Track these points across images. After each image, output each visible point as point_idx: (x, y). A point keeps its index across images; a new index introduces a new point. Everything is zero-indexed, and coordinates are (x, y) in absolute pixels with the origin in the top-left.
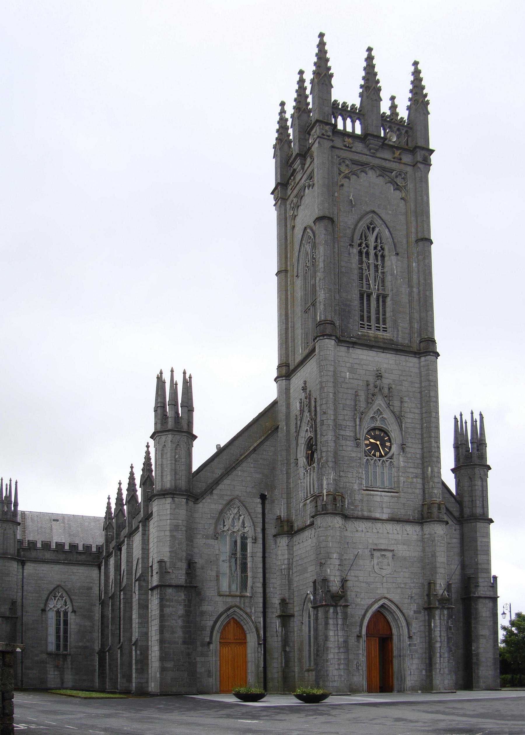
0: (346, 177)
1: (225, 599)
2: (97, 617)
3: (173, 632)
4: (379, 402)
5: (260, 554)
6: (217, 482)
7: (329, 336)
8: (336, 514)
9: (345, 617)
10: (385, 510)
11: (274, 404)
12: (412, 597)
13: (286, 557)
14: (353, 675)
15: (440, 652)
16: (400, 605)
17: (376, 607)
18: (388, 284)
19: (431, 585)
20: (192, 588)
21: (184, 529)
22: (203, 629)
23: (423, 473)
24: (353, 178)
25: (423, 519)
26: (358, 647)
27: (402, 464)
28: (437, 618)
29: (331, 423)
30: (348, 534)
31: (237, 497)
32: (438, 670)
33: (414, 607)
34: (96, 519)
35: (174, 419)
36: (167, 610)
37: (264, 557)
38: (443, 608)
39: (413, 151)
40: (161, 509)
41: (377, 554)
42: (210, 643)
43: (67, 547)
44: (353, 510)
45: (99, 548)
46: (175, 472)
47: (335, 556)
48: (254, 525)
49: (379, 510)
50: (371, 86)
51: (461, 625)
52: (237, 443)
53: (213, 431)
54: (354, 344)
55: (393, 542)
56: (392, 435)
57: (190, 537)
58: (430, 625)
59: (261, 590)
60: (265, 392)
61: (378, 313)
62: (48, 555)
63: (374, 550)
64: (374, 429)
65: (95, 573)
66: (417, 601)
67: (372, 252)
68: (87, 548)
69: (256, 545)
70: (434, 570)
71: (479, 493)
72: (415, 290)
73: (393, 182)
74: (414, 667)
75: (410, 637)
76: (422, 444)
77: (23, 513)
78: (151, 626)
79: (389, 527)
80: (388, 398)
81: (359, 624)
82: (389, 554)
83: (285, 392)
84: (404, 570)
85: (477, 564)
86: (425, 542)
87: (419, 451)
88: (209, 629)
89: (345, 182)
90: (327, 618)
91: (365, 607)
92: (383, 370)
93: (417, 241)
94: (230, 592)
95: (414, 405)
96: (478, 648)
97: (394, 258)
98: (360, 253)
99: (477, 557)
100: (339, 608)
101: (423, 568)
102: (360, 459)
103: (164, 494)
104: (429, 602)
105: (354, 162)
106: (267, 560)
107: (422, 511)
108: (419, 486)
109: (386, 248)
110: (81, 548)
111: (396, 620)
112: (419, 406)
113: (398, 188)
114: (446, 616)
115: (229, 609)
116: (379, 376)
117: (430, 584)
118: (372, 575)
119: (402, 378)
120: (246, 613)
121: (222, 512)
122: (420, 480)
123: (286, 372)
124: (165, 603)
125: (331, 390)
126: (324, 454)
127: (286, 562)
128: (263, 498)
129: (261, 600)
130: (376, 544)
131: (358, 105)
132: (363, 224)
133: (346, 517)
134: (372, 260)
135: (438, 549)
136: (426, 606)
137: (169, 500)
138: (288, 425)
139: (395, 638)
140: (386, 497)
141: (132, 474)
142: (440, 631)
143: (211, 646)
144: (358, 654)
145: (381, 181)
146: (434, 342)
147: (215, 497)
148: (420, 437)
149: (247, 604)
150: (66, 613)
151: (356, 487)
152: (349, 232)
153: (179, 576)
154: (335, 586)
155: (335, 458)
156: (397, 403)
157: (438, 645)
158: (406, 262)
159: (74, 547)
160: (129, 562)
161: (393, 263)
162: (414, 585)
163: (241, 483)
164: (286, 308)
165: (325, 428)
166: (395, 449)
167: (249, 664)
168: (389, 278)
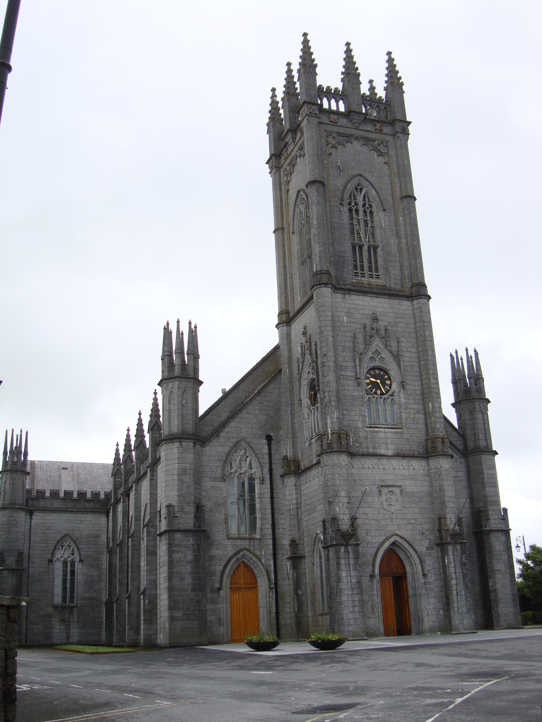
0: (334, 147)
2: (105, 566)
3: (182, 579)
4: (377, 343)
5: (268, 495)
6: (224, 425)
7: (326, 284)
10: (390, 446)
11: (277, 348)
12: (423, 533)
14: (368, 618)
16: (412, 542)
19: (441, 519)
20: (201, 532)
21: (192, 472)
22: (212, 574)
24: (341, 159)
25: (428, 453)
27: (403, 401)
28: (450, 553)
29: (332, 364)
30: (355, 471)
32: (456, 609)
33: (426, 543)
34: (104, 466)
35: (180, 366)
36: (176, 556)
37: (272, 498)
38: (456, 543)
39: (392, 123)
40: (169, 454)
41: (385, 490)
42: (220, 589)
43: (75, 495)
44: (358, 447)
45: (107, 495)
46: (182, 417)
47: (343, 494)
48: (261, 466)
49: (384, 446)
50: (351, 72)
51: (476, 560)
52: (241, 386)
53: (218, 377)
54: (349, 291)
55: (400, 478)
56: (392, 373)
57: (198, 481)
58: (444, 562)
59: (270, 531)
60: (269, 338)
61: (370, 262)
62: (56, 504)
63: (382, 486)
64: (374, 368)
65: (103, 520)
66: (429, 537)
67: (361, 209)
68: (96, 495)
70: (443, 504)
71: (480, 426)
74: (431, 607)
75: (424, 575)
76: (421, 380)
77: (33, 463)
78: (160, 573)
79: (395, 462)
81: (371, 563)
82: (397, 490)
83: (286, 337)
85: (485, 496)
86: (432, 477)
87: (419, 388)
88: (218, 574)
89: (333, 151)
90: (338, 558)
91: (377, 545)
92: (378, 314)
93: (402, 198)
94: (239, 535)
95: (410, 345)
96: (495, 583)
97: (381, 214)
98: (350, 210)
99: (485, 490)
100: (350, 547)
101: (432, 503)
102: (362, 397)
103: (171, 438)
104: (441, 538)
106: (276, 501)
107: (427, 446)
108: (422, 421)
109: (374, 205)
110: (89, 496)
111: (409, 557)
112: (415, 345)
113: (380, 154)
114: (459, 551)
115: (238, 552)
116: (375, 319)
117: (440, 518)
118: (381, 512)
119: (397, 320)
120: (256, 556)
121: (228, 454)
122: (422, 416)
123: (286, 319)
124: (173, 548)
125: (330, 333)
126: (327, 394)
128: (269, 438)
129: (270, 542)
130: (383, 481)
131: (340, 88)
132: (351, 186)
133: (351, 455)
134: (361, 216)
135: (445, 483)
136: (438, 542)
137: (177, 444)
138: (290, 368)
139: (409, 576)
140: (390, 434)
141: (140, 420)
143: (221, 592)
144: (372, 595)
145: (365, 149)
146: (425, 286)
147: (222, 440)
148: (418, 374)
149: (257, 547)
150: (73, 563)
151: (360, 425)
152: (339, 193)
153: (187, 521)
156: (394, 344)
157: (454, 582)
159: (82, 494)
160: (137, 508)
161: (381, 219)
163: (247, 425)
164: (284, 261)
165: (326, 369)
168: (378, 231)
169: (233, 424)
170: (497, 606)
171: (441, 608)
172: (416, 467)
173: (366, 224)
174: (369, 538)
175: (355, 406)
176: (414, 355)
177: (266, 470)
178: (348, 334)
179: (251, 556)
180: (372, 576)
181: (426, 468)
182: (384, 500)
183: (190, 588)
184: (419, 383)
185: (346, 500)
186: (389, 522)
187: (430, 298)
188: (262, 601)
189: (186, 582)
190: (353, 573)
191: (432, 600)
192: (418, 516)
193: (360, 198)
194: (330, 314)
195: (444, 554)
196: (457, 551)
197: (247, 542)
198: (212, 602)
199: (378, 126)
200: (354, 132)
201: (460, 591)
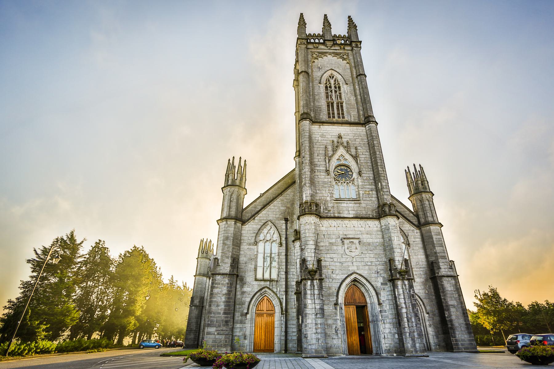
1: (259, 283)
3: (218, 306)
4: (341, 151)
5: (284, 254)
6: (258, 213)
8: (312, 214)
9: (321, 288)
10: (350, 212)
11: (294, 170)
12: (378, 272)
13: (299, 254)
14: (332, 339)
15: (407, 317)
16: (369, 279)
17: (348, 280)
18: (343, 97)
19: (391, 261)
21: (232, 238)
22: (243, 303)
23: (376, 188)
25: (379, 215)
26: (336, 314)
27: (360, 184)
28: (400, 287)
29: (308, 161)
31: (270, 221)
32: (408, 334)
33: (381, 280)
36: (215, 291)
37: (286, 255)
38: (403, 279)
41: (346, 241)
42: (247, 313)
44: (327, 213)
48: (280, 236)
49: (346, 212)
51: (434, 297)
55: (359, 233)
56: (352, 168)
58: (395, 294)
59: (284, 276)
63: (344, 238)
66: (383, 275)
69: (281, 248)
70: (392, 250)
72: (359, 97)
73: (341, 57)
74: (387, 331)
75: (380, 304)
76: (373, 171)
79: (355, 222)
80: (347, 147)
81: (335, 294)
82: (356, 241)
84: (370, 252)
86: (385, 231)
87: (372, 175)
88: (247, 304)
89: (316, 61)
91: (340, 281)
92: (342, 135)
95: (364, 151)
96: (450, 315)
97: (345, 86)
98: (326, 87)
99: (435, 249)
100: (315, 282)
101: (385, 250)
102: (331, 182)
104: (392, 275)
105: (319, 53)
106: (289, 257)
107: (379, 211)
108: (375, 196)
109: (341, 83)
112: (368, 151)
113: (344, 59)
114: (407, 286)
115: (261, 289)
117: (390, 260)
118: (343, 256)
119: (355, 137)
120: (274, 292)
122: (374, 192)
124: (214, 285)
125: (308, 145)
126: (303, 180)
127: (299, 257)
128: (286, 220)
129: (284, 283)
130: (346, 235)
135: (392, 235)
136: (390, 278)
139: (369, 305)
140: (351, 205)
142: (404, 298)
143: (248, 315)
144: (336, 320)
147: (256, 221)
148: (371, 167)
149: (274, 286)
151: (328, 199)
152: (319, 78)
153: (226, 268)
154: (311, 265)
155: (310, 181)
157: (404, 310)
158: (352, 87)
162: (378, 263)
165: (304, 165)
166: (355, 175)
167: (276, 329)
169: (264, 212)
170: (454, 333)
171: (395, 333)
172: (371, 226)
173: (336, 92)
174: (334, 276)
175: (326, 187)
176: (368, 156)
177: (283, 239)
178: (322, 146)
179: (270, 292)
180: (336, 304)
181: (379, 226)
182: (346, 248)
183: (222, 312)
184: (372, 172)
185: (313, 247)
186: (350, 264)
187: (442, 226)
188: (277, 324)
189: (220, 308)
190: (317, 301)
191: (387, 326)
192: (374, 260)
193: (332, 81)
194: (308, 134)
195: (394, 286)
196: (405, 285)
197: (268, 283)
198: (242, 322)
199: (342, 47)
200: (328, 51)
201: (411, 319)
